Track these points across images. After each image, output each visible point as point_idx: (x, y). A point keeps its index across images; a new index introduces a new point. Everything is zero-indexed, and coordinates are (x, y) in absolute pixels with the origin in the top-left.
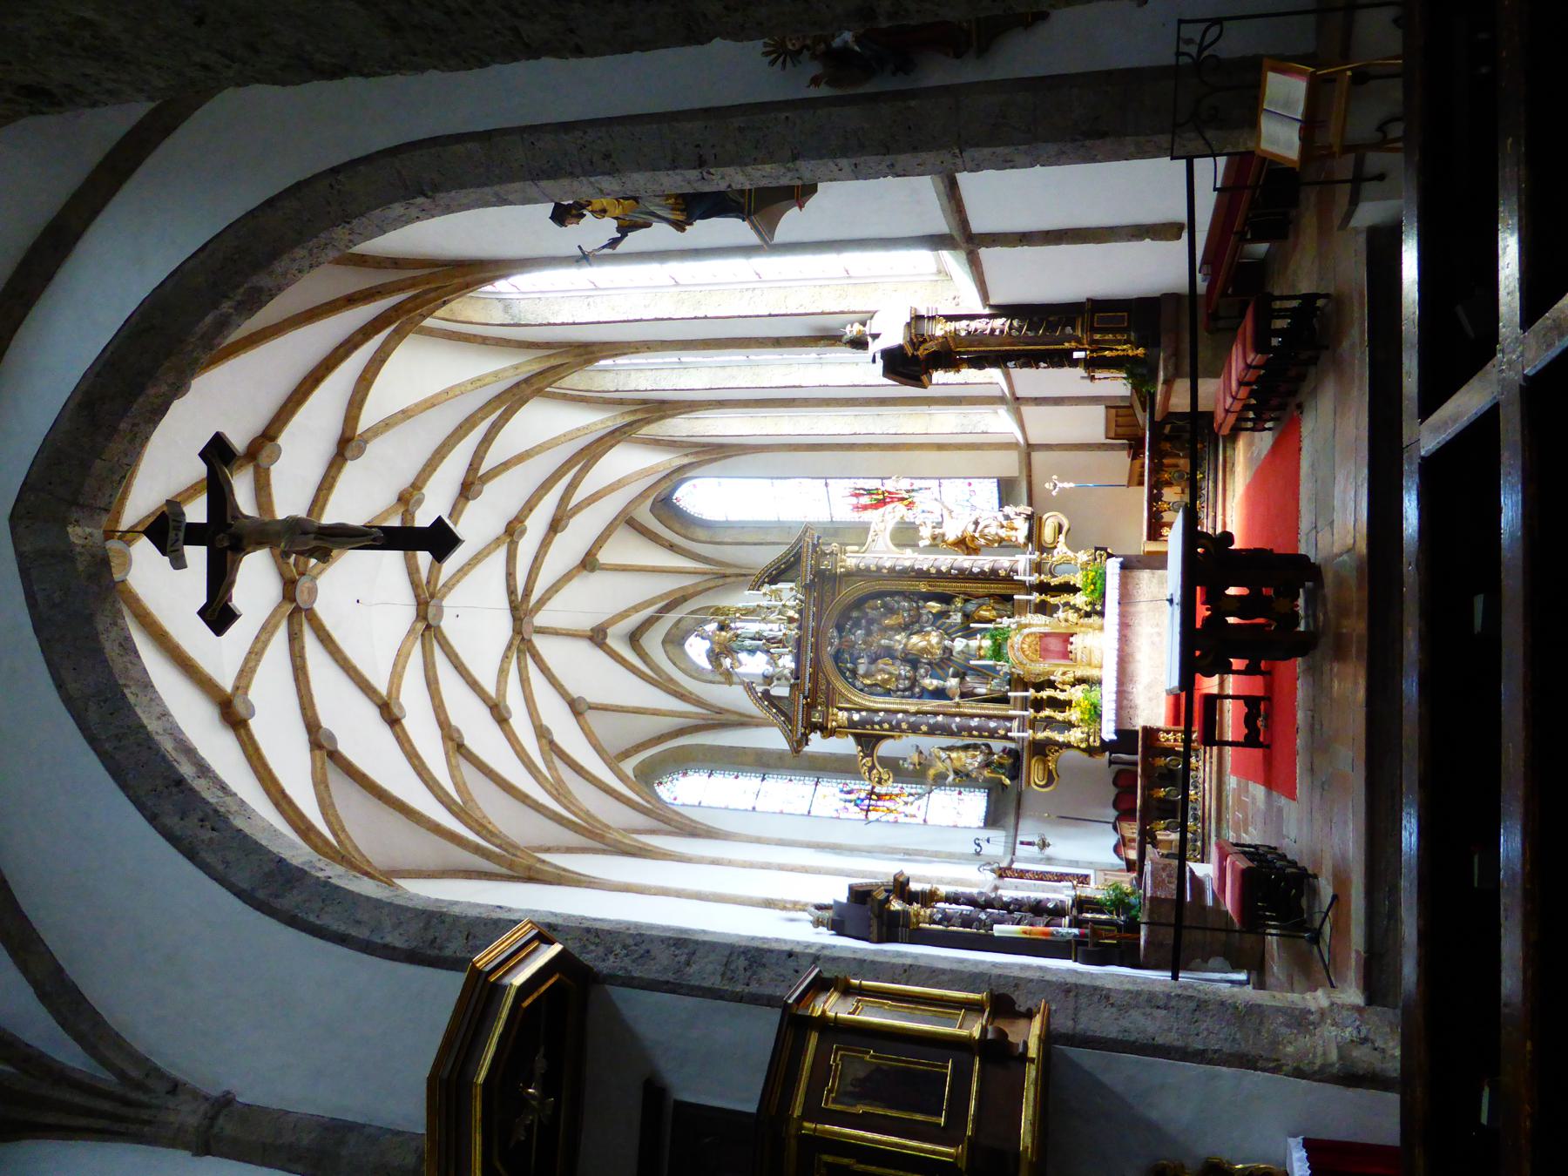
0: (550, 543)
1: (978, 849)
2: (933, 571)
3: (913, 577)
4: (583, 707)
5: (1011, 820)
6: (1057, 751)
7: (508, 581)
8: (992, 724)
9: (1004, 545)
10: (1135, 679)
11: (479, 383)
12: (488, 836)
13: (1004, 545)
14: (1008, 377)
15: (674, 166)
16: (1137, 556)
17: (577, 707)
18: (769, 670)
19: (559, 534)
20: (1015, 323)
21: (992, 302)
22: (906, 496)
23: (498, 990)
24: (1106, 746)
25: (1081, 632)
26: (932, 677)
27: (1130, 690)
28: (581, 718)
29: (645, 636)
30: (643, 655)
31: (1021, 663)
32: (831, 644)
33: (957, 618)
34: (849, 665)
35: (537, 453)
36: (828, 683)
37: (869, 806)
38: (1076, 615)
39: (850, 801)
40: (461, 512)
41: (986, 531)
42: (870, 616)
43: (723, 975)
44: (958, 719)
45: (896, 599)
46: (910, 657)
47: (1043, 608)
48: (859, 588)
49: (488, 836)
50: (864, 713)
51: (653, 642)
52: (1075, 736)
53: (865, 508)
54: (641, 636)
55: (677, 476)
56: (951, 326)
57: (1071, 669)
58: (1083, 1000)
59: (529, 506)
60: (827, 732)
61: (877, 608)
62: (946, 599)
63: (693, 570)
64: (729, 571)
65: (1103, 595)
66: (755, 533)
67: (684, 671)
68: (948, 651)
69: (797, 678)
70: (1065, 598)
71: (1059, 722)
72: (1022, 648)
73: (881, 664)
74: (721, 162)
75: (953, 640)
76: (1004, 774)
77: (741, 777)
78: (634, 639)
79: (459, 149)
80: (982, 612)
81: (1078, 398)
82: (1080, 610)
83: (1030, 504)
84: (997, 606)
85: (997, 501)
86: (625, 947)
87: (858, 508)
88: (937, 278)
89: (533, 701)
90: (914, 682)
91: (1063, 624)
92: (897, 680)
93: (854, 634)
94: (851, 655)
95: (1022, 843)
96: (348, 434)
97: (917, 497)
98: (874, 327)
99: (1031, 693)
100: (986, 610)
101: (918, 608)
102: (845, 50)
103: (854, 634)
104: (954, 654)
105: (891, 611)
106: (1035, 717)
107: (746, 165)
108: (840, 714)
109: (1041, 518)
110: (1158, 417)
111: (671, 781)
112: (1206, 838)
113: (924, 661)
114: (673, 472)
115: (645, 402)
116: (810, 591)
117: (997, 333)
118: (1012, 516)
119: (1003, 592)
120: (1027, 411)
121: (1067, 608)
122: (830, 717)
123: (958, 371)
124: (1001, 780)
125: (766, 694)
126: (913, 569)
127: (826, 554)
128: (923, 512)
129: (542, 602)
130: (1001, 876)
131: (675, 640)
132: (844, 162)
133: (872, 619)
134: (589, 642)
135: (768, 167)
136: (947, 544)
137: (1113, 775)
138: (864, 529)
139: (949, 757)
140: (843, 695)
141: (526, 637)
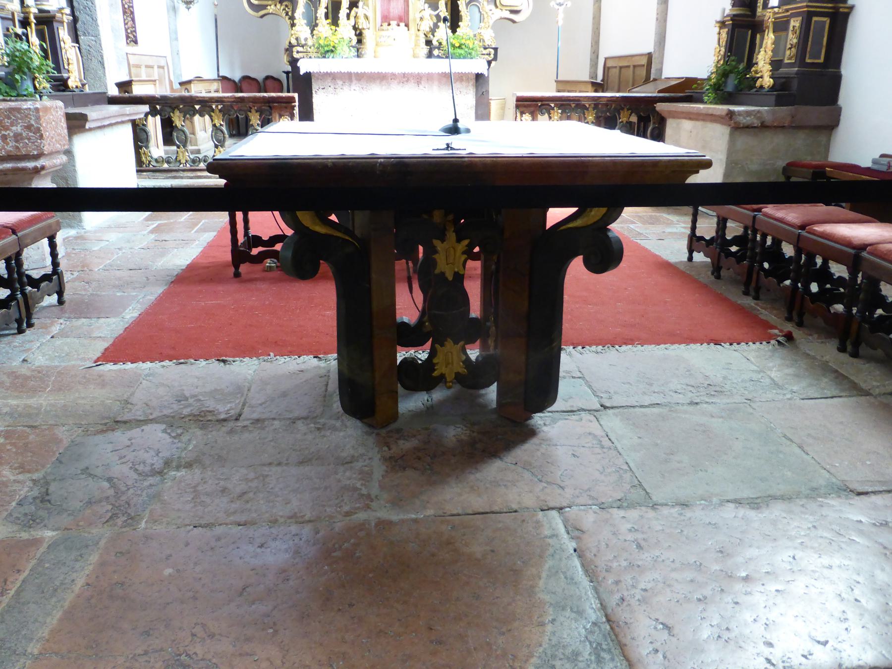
6: (287, 14)
16: (487, 92)
24: (294, 62)
27: (353, 87)
38: (428, 29)
52: (302, 30)
57: (371, 25)
71: (316, 12)
81: (665, 21)
91: (418, 16)
110: (660, 107)
112: (174, 174)
121: (435, 20)
137: (275, 76)
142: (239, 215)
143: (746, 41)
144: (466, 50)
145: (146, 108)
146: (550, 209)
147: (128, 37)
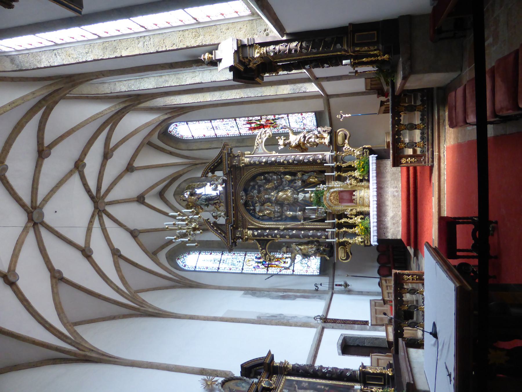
1: (317, 288)
2: (286, 162)
4: (137, 233)
5: (331, 271)
9: (317, 146)
10: (386, 214)
11: (14, 105)
12: (65, 339)
13: (317, 146)
17: (134, 234)
18: (274, 118)
20: (304, 44)
21: (288, 31)
25: (358, 189)
26: (290, 211)
29: (166, 193)
31: (330, 206)
32: (242, 199)
33: (299, 183)
35: (78, 129)
36: (243, 217)
37: (268, 264)
39: (260, 263)
40: (41, 165)
41: (310, 140)
42: (259, 184)
45: (271, 175)
46: (279, 202)
48: (254, 171)
49: (65, 339)
51: (170, 195)
52: (358, 239)
53: (255, 128)
56: (264, 50)
59: (85, 152)
61: (261, 180)
63: (181, 164)
65: (368, 172)
70: (349, 173)
72: (330, 199)
75: (298, 195)
76: (326, 255)
77: (213, 253)
78: (161, 195)
83: (331, 125)
87: (251, 129)
88: (251, 18)
90: (282, 213)
91: (350, 186)
92: (274, 213)
93: (253, 192)
95: (336, 285)
97: (278, 122)
98: (218, 54)
99: (336, 220)
100: (312, 179)
101: (281, 178)
103: (253, 192)
105: (268, 181)
106: (339, 232)
109: (336, 132)
111: (183, 258)
113: (286, 203)
115: (129, 96)
116: (229, 176)
117: (293, 52)
118: (322, 132)
121: (351, 177)
122: (244, 234)
124: (325, 257)
125: (215, 223)
129: (108, 191)
130: (325, 322)
133: (260, 185)
134: (137, 202)
136: (292, 148)
138: (253, 138)
144: (365, 165)
145: (400, 340)
146: (474, 242)
147: (365, 324)
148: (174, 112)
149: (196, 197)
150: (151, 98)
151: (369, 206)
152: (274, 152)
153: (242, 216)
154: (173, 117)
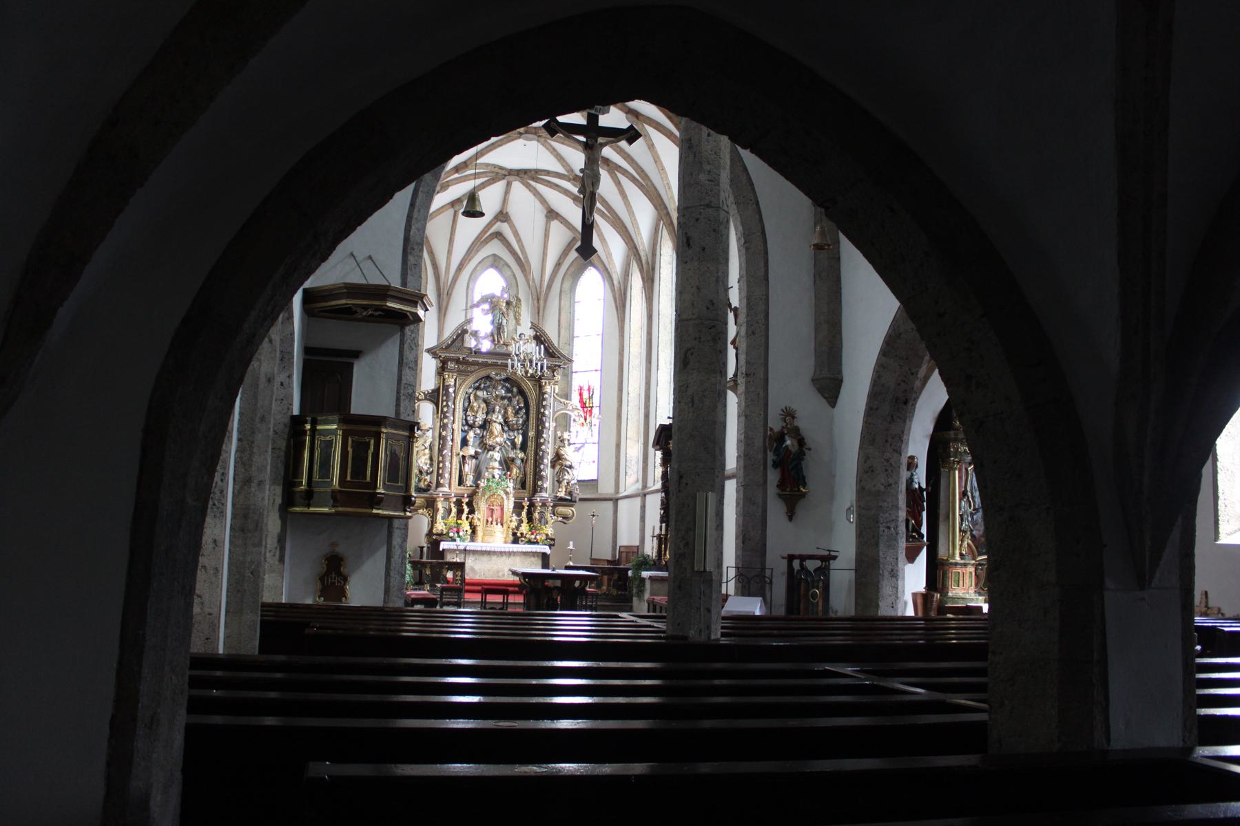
0: (567, 196)
2: (542, 440)
3: (538, 428)
6: (429, 515)
7: (544, 171)
8: (447, 475)
14: (657, 491)
15: (748, 363)
19: (572, 201)
22: (588, 421)
23: (415, 304)
25: (504, 530)
28: (450, 206)
30: (487, 241)
34: (483, 385)
35: (625, 203)
36: (472, 372)
43: (406, 384)
44: (450, 454)
47: (518, 507)
50: (453, 395)
53: (581, 395)
54: (499, 240)
55: (606, 273)
57: (481, 524)
58: (403, 531)
60: (441, 371)
61: (518, 404)
62: (524, 447)
64: (542, 302)
66: (567, 326)
67: (475, 269)
68: (492, 448)
69: (475, 353)
70: (525, 520)
73: (483, 405)
74: (747, 383)
79: (762, 264)
80: (515, 470)
82: (517, 530)
84: (519, 479)
85: (583, 479)
86: (414, 338)
89: (465, 181)
90: (472, 427)
94: (489, 387)
96: (640, 117)
97: (586, 428)
101: (518, 430)
102: (784, 441)
104: (490, 452)
105: (516, 413)
107: (745, 395)
108: (453, 380)
113: (485, 433)
114: (609, 273)
115: (653, 269)
119: (528, 483)
120: (638, 501)
122: (451, 374)
123: (661, 466)
126: (544, 427)
127: (553, 372)
128: (577, 432)
131: (496, 262)
132: (743, 437)
135: (744, 404)
139: (426, 448)
140: (464, 381)
141: (507, 177)
142: (506, 596)
143: (970, 643)
148: (621, 294)
149: (505, 310)
150: (648, 296)
151: (482, 542)
152: (554, 424)
153: (473, 372)
154: (613, 290)
